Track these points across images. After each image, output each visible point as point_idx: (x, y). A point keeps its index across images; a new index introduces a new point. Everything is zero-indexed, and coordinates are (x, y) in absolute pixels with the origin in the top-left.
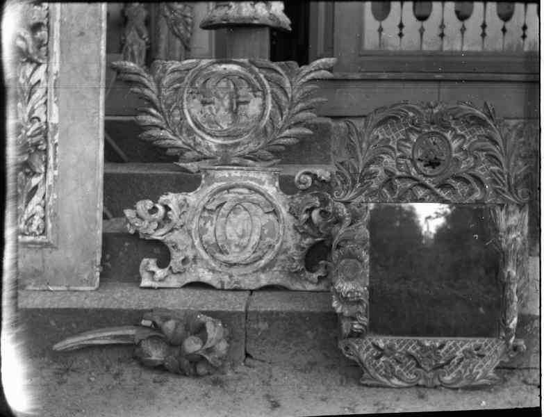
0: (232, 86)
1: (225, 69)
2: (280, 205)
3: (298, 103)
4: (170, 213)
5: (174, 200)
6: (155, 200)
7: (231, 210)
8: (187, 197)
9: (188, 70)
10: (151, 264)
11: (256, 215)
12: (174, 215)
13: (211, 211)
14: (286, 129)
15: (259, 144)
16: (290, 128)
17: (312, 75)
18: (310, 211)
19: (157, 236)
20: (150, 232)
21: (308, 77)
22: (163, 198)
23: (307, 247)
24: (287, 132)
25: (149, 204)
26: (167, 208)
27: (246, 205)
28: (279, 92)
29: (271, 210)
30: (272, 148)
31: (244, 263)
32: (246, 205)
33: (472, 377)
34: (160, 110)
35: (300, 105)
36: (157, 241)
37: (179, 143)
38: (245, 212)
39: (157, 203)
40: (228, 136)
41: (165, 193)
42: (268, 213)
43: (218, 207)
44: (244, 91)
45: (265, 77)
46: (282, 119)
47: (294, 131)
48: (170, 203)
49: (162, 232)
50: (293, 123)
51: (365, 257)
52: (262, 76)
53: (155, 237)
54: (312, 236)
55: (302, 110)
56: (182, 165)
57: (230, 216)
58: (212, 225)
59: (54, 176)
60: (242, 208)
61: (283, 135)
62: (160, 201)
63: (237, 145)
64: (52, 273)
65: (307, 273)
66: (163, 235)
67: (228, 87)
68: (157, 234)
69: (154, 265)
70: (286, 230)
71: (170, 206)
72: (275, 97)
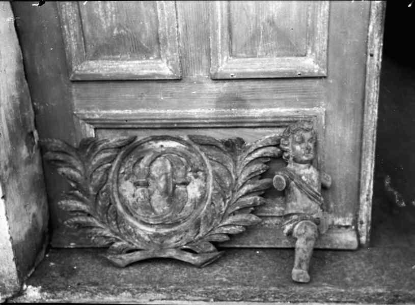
0: (169, 167)
1: (162, 146)
3: (244, 184)
14: (230, 215)
15: (198, 233)
16: (234, 214)
17: (260, 152)
21: (256, 155)
33: (94, 195)
35: (246, 188)
40: (163, 225)
45: (205, 154)
46: (225, 205)
47: (239, 217)
50: (238, 208)
51: (92, 220)
52: (203, 154)
55: (248, 193)
56: (109, 257)
59: (214, 301)
61: (226, 223)
63: (135, 45)
64: (309, 242)
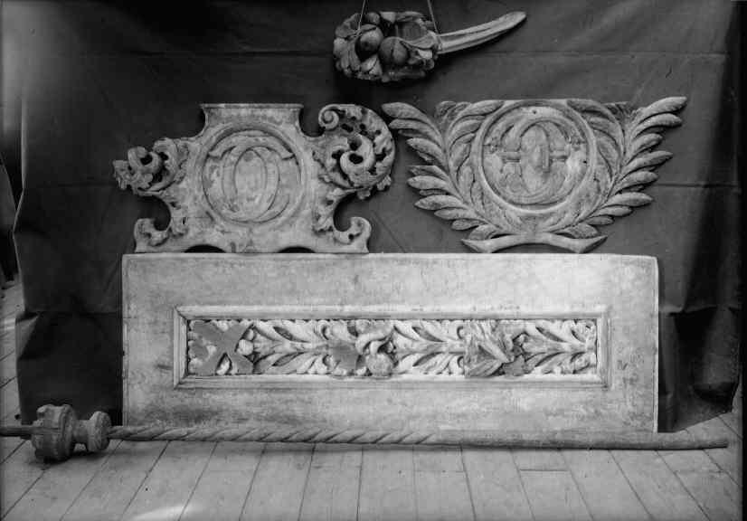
2: (301, 149)
4: (166, 162)
5: (173, 146)
6: (149, 149)
7: (242, 155)
8: (188, 142)
9: (485, 115)
10: (147, 224)
11: (271, 162)
12: (171, 163)
13: (215, 158)
18: (337, 156)
19: (153, 190)
20: (144, 187)
22: (158, 144)
23: (335, 200)
24: (617, 199)
25: (142, 151)
26: (164, 157)
27: (259, 150)
28: (609, 145)
29: (289, 155)
30: (597, 220)
31: (260, 220)
32: (259, 150)
34: (446, 168)
36: (154, 197)
37: (470, 213)
38: (258, 158)
39: (152, 150)
41: (161, 138)
42: (286, 159)
43: (224, 153)
44: (559, 142)
47: (627, 196)
48: (166, 149)
49: (158, 186)
53: (149, 193)
54: (343, 188)
57: (240, 163)
58: (218, 175)
60: (254, 154)
62: (155, 147)
63: (544, 217)
65: (336, 231)
66: (158, 191)
67: (538, 138)
68: (152, 189)
69: (150, 227)
70: (309, 179)
71: (167, 153)
72: (601, 147)
